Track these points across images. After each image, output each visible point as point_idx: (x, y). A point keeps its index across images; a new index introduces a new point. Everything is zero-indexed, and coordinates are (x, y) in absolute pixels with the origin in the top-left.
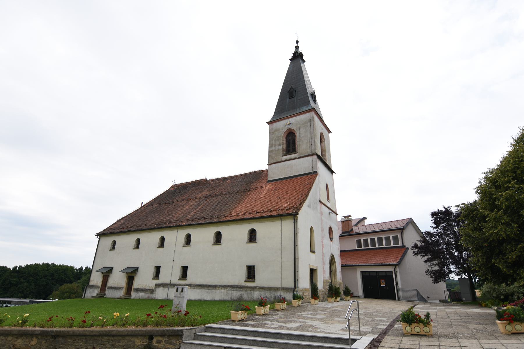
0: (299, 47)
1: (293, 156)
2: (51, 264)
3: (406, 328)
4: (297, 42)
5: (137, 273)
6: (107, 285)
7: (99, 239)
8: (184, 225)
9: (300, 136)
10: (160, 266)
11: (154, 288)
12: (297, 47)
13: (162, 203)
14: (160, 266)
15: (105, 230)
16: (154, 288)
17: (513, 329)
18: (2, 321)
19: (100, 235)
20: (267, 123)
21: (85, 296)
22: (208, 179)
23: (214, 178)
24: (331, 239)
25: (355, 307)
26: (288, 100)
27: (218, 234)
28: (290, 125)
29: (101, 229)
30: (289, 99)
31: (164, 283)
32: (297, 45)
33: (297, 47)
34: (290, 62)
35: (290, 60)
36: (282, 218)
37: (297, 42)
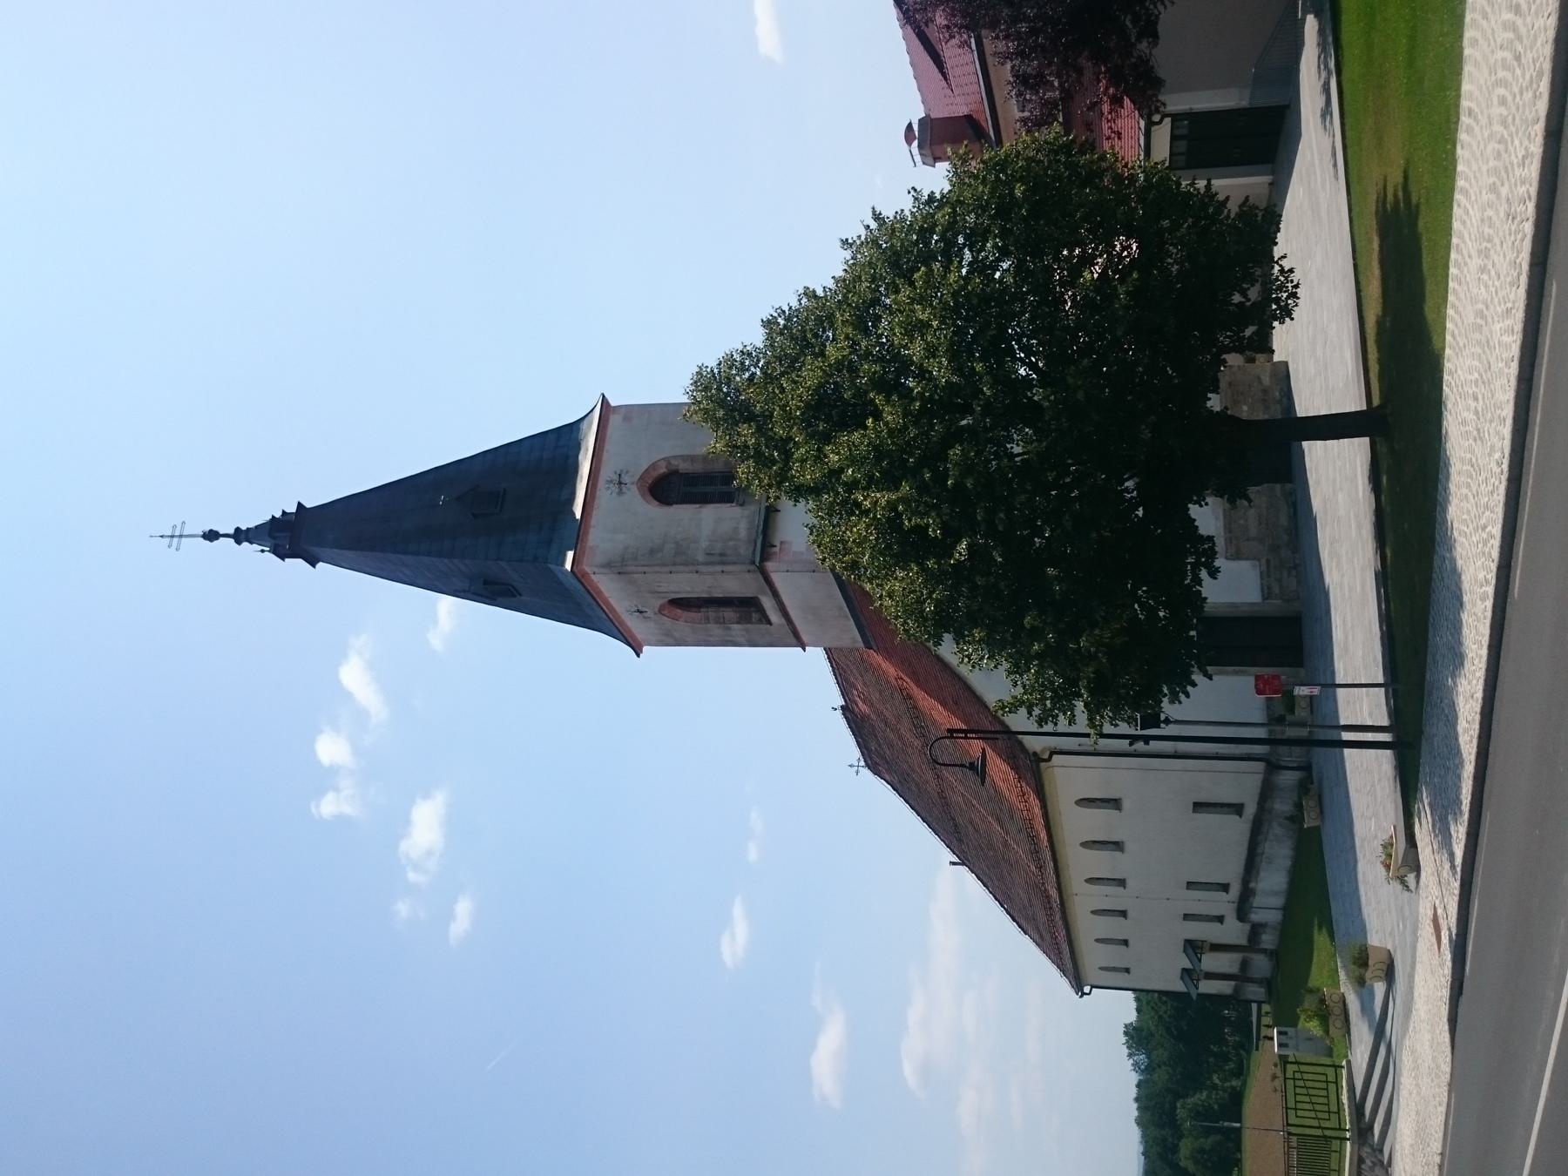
0: (238, 529)
1: (768, 603)
2: (1151, 742)
3: (1336, 1013)
4: (211, 536)
5: (1202, 941)
8: (1044, 806)
11: (1250, 924)
12: (240, 536)
15: (1064, 972)
16: (1250, 924)
18: (1487, 258)
19: (1078, 985)
20: (638, 656)
25: (1346, 674)
26: (523, 598)
29: (1063, 985)
30: (520, 595)
33: (240, 536)
34: (320, 565)
35: (313, 565)
37: (211, 536)
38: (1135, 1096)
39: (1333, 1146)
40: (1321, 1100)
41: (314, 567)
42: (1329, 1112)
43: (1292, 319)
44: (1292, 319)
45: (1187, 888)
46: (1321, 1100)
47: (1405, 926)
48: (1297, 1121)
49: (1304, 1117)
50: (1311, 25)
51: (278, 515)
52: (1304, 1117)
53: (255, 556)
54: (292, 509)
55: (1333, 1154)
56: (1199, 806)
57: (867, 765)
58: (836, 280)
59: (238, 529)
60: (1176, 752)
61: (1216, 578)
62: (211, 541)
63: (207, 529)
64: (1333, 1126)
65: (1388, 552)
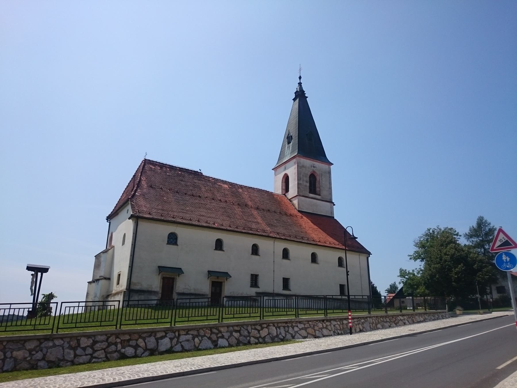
0: (301, 83)
4: (300, 78)
6: (174, 290)
7: (110, 223)
9: (322, 182)
10: (283, 278)
12: (300, 84)
13: (189, 193)
14: (283, 278)
17: (144, 355)
21: (87, 303)
22: (204, 174)
23: (165, 162)
24: (123, 244)
27: (176, 235)
28: (315, 168)
31: (266, 292)
32: (300, 81)
33: (300, 84)
36: (361, 254)
37: (300, 78)
38: (377, 288)
40: (146, 316)
42: (79, 307)
43: (371, 254)
44: (371, 254)
45: (252, 275)
46: (146, 316)
48: (170, 317)
51: (305, 93)
53: (295, 87)
54: (306, 95)
59: (301, 83)
61: (31, 275)
62: (299, 78)
63: (299, 79)
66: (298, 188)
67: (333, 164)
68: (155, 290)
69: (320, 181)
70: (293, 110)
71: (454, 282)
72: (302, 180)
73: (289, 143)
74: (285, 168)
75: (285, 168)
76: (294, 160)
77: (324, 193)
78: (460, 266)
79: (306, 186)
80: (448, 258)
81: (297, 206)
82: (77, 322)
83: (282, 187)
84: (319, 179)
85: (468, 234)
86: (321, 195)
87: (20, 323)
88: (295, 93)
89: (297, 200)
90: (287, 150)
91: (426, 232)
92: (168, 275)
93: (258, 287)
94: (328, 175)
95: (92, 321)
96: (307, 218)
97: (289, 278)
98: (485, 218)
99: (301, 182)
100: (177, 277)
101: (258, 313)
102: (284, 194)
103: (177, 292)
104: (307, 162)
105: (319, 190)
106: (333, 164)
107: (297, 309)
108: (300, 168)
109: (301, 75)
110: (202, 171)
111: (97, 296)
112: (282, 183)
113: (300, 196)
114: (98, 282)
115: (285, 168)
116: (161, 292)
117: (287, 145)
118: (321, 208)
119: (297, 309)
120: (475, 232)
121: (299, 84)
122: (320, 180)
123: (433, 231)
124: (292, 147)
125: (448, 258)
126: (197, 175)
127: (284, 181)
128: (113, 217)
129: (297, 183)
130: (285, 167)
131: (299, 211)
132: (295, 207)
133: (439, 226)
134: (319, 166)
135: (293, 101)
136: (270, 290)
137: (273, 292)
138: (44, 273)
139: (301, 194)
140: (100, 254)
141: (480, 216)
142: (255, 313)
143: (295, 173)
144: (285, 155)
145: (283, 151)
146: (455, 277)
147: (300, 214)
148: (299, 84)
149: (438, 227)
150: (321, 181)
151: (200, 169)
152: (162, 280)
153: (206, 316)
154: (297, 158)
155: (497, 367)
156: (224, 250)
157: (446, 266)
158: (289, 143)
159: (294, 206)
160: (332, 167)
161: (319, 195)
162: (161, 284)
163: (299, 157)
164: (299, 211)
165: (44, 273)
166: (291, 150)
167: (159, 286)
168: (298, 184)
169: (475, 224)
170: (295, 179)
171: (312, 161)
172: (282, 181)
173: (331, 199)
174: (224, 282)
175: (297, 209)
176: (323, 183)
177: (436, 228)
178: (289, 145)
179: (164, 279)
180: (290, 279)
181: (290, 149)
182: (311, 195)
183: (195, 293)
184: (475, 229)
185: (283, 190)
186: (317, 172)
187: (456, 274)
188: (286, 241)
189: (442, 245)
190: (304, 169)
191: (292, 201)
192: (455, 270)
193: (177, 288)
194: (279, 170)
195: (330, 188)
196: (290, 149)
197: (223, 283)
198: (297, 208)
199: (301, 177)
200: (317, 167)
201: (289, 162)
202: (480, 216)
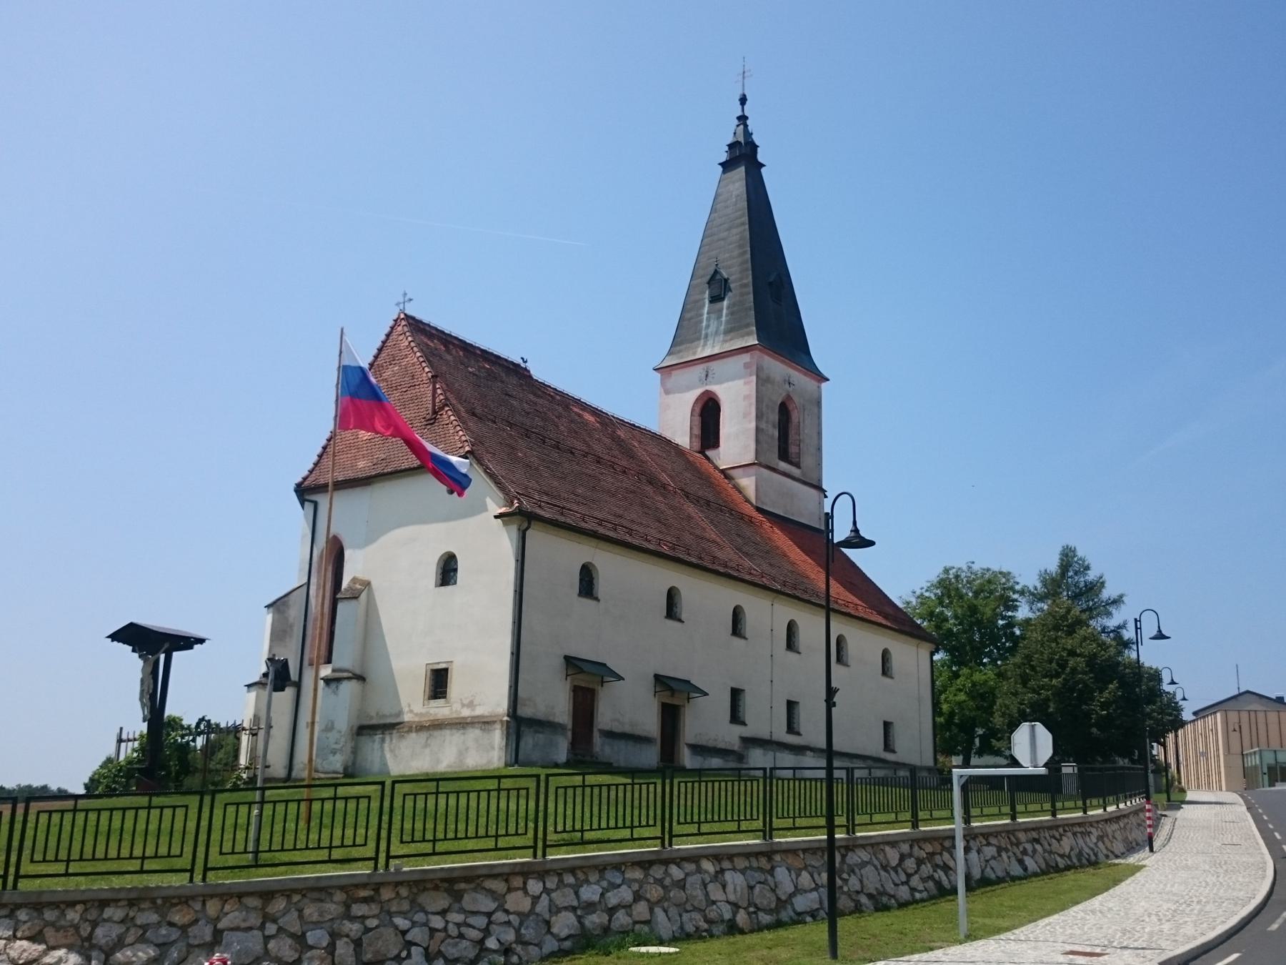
0: (747, 118)
4: (743, 100)
12: (743, 119)
33: (743, 119)
37: (743, 100)
39: (976, 809)
41: (720, 164)
47: (841, 605)
49: (186, 820)
50: (678, 950)
52: (186, 820)
53: (728, 132)
55: (893, 815)
56: (887, 725)
57: (518, 366)
58: (1143, 664)
59: (747, 118)
60: (572, 840)
63: (739, 103)
64: (210, 858)
65: (588, 417)
66: (758, 441)
67: (828, 380)
68: (561, 722)
69: (799, 426)
70: (721, 198)
71: (1097, 725)
72: (765, 419)
73: (715, 299)
74: (707, 376)
75: (704, 374)
76: (746, 358)
77: (807, 461)
78: (1111, 686)
79: (772, 437)
80: (1080, 663)
81: (751, 494)
82: (332, 801)
83: (691, 429)
84: (797, 420)
85: (1032, 590)
86: (802, 465)
87: (348, 805)
88: (731, 146)
89: (753, 478)
90: (708, 320)
91: (941, 576)
92: (583, 681)
93: (744, 724)
94: (816, 410)
95: (418, 797)
96: (782, 530)
97: (798, 703)
98: (1080, 553)
99: (763, 426)
100: (600, 687)
101: (557, 788)
102: (702, 452)
103: (599, 727)
104: (778, 368)
105: (797, 451)
106: (828, 380)
107: (768, 780)
108: (762, 385)
109: (746, 93)
110: (530, 366)
111: (336, 725)
112: (692, 415)
113: (760, 465)
114: (337, 687)
115: (707, 376)
116: (570, 726)
117: (707, 302)
118: (802, 506)
119: (768, 780)
120: (1053, 586)
121: (739, 118)
122: (799, 422)
123: (957, 577)
124: (731, 313)
125: (1080, 663)
126: (518, 372)
127: (698, 410)
128: (345, 488)
129: (753, 425)
130: (707, 372)
131: (759, 510)
132: (744, 496)
133: (973, 563)
134: (801, 379)
135: (720, 169)
136: (764, 734)
137: (769, 738)
138: (175, 654)
139: (762, 460)
140: (286, 599)
141: (1067, 546)
142: (566, 788)
143: (747, 397)
144: (703, 332)
145: (690, 319)
146: (1102, 715)
147: (760, 517)
148: (739, 118)
149: (970, 564)
150: (801, 424)
151: (522, 358)
152: (572, 694)
153: (443, 793)
154: (757, 352)
155: (1269, 926)
156: (683, 619)
157: (1078, 683)
158: (715, 299)
159: (740, 492)
160: (824, 385)
161: (798, 466)
162: (571, 708)
163: (760, 350)
164: (759, 510)
165: (175, 654)
166: (727, 322)
167: (567, 709)
168: (758, 430)
169: (1053, 566)
170: (746, 415)
171: (786, 364)
172: (693, 410)
173: (820, 480)
174: (684, 706)
175: (751, 503)
176: (806, 431)
177: (965, 568)
178: (718, 305)
179: (576, 690)
180: (801, 704)
181: (724, 319)
182: (783, 466)
183: (631, 732)
184: (1053, 580)
185: (694, 439)
186: (796, 399)
187: (1104, 706)
188: (796, 601)
189: (1056, 628)
190: (769, 386)
191: (733, 479)
192: (1102, 698)
193: (599, 720)
194: (679, 377)
195: (819, 449)
196: (724, 319)
197: (682, 709)
198: (753, 501)
199: (764, 410)
200: (795, 383)
201: (723, 357)
202: (1067, 546)
